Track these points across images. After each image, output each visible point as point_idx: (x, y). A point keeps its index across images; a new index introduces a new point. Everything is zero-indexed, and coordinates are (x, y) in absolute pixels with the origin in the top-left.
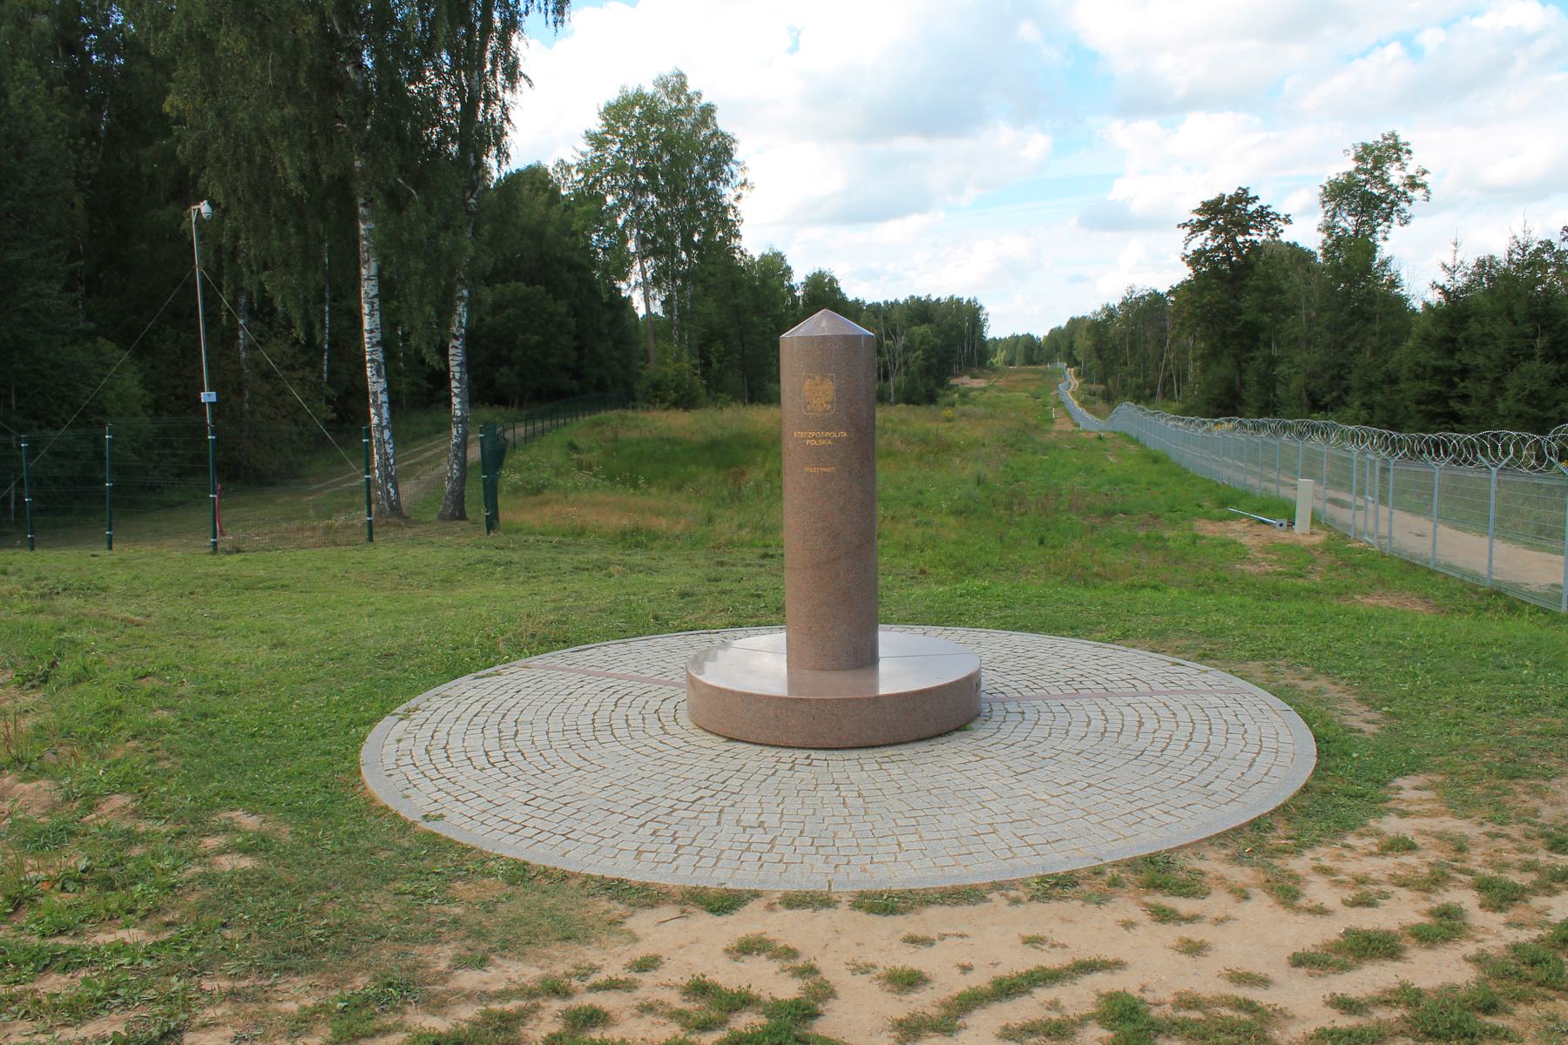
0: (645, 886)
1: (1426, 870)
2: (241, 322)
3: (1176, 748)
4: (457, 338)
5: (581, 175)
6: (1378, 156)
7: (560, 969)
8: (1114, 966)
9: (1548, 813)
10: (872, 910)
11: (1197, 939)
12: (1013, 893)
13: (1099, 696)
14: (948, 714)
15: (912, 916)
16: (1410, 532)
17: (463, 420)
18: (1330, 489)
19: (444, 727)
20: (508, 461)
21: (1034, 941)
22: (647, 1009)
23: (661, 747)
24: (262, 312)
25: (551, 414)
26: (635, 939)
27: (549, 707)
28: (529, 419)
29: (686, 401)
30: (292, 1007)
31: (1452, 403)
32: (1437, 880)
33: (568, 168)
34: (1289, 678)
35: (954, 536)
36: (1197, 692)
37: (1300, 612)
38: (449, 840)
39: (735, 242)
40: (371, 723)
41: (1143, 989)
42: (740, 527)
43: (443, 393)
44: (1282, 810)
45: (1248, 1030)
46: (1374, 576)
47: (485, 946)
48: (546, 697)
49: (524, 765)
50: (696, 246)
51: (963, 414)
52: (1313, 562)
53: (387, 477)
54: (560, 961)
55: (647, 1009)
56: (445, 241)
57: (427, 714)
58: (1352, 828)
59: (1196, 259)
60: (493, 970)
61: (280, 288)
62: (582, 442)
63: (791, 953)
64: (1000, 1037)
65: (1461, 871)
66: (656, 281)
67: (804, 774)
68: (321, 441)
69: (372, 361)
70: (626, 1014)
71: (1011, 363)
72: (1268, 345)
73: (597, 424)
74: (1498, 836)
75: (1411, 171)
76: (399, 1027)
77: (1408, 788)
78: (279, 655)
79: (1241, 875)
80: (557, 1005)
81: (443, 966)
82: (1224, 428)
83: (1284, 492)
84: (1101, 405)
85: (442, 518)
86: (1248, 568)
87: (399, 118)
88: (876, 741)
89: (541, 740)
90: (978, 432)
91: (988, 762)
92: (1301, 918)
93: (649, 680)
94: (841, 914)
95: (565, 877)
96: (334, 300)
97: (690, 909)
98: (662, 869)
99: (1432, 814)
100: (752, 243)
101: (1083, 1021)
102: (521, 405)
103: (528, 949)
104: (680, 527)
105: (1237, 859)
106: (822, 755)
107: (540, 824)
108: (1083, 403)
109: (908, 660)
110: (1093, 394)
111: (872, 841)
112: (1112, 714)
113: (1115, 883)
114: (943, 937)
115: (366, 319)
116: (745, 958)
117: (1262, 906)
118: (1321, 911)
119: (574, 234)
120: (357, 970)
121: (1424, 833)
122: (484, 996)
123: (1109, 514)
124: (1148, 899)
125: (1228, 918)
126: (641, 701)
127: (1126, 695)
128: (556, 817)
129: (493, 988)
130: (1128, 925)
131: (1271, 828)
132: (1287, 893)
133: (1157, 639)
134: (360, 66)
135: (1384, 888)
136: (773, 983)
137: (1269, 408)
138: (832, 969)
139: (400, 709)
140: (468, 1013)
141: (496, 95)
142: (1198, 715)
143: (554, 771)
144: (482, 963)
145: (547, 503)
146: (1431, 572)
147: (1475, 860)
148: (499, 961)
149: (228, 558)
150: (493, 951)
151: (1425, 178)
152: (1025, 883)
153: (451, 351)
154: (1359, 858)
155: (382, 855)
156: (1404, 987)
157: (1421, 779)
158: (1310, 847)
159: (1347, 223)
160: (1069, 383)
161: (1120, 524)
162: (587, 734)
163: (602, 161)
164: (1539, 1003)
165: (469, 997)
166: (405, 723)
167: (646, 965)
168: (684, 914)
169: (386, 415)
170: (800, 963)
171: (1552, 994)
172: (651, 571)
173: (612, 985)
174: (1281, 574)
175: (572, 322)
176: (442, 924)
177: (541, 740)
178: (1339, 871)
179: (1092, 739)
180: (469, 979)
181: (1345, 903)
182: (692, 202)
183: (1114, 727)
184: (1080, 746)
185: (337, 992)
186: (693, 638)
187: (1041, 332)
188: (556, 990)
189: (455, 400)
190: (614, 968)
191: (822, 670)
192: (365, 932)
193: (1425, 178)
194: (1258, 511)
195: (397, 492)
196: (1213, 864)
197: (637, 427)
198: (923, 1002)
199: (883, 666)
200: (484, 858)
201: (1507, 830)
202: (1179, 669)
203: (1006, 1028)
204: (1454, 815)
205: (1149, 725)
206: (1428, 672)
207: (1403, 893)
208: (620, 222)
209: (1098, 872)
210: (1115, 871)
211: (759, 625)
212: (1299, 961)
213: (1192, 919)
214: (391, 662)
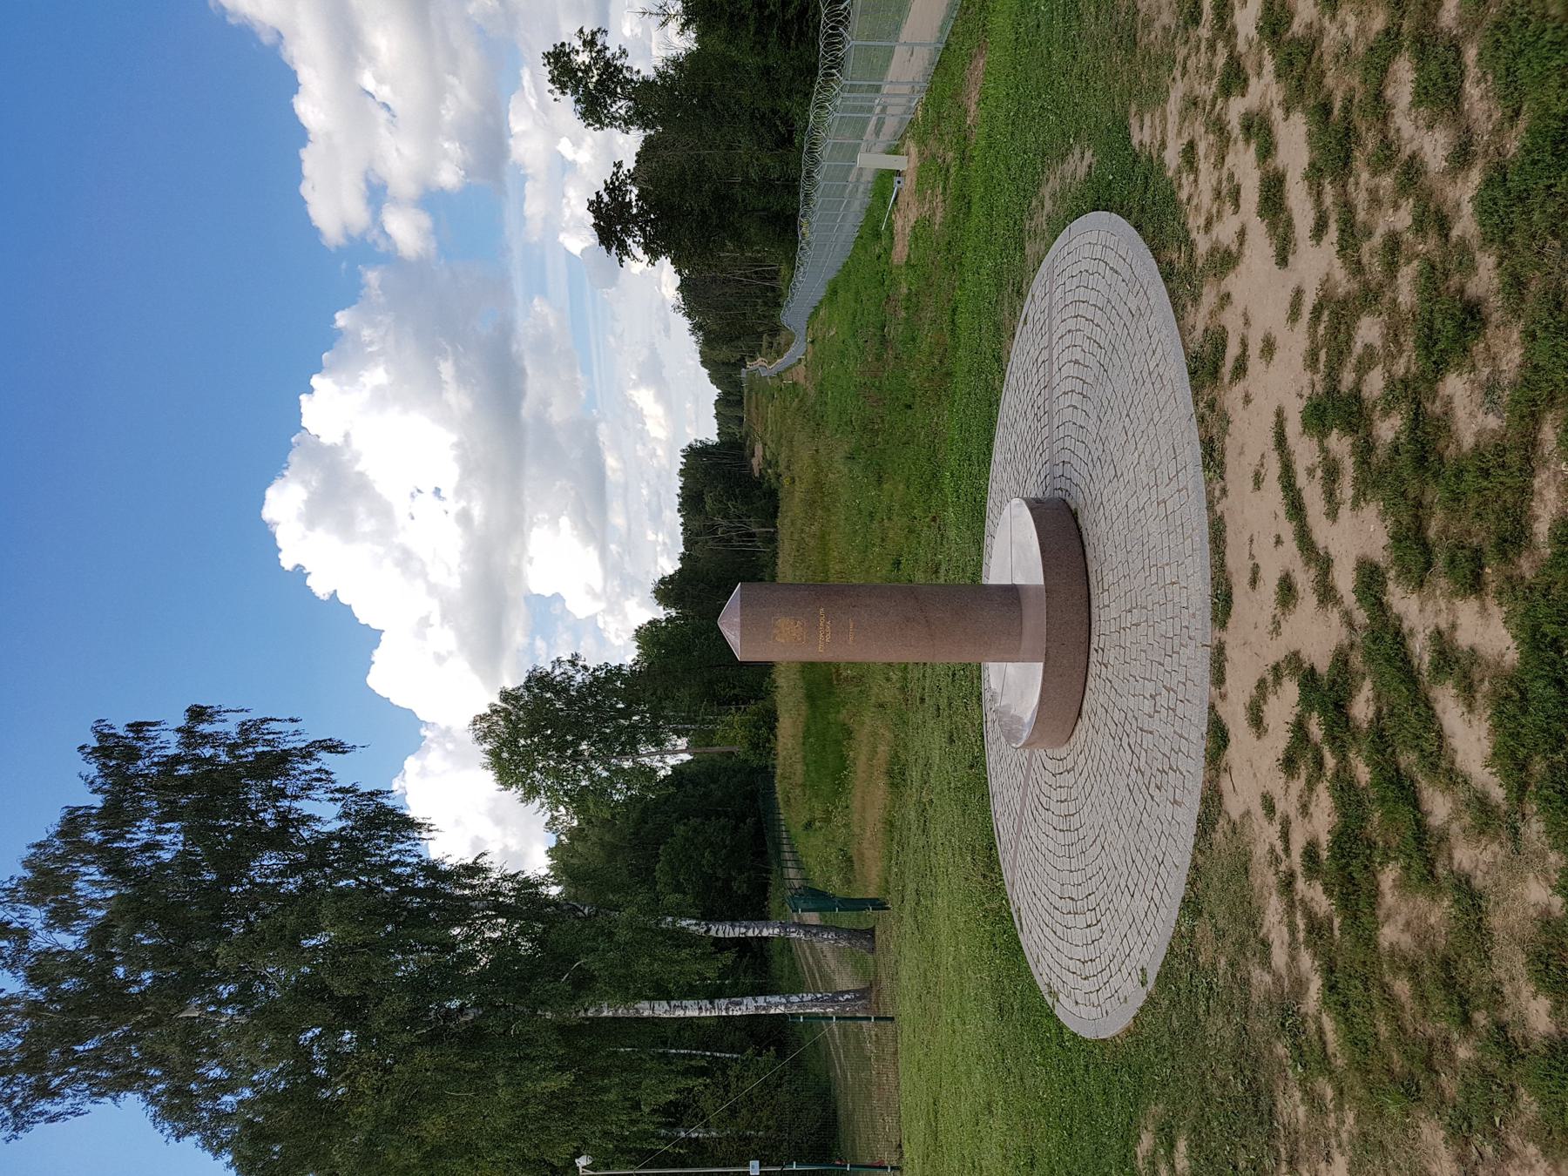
0: (1204, 800)
1: (1211, 137)
2: (683, 1134)
3: (1097, 334)
4: (709, 930)
5: (561, 808)
6: (561, 67)
7: (1272, 880)
8: (1279, 414)
9: (1166, 18)
10: (1227, 614)
11: (1261, 345)
12: (1217, 493)
13: (1051, 394)
14: (1061, 526)
15: (1234, 580)
16: (907, 67)
17: (783, 926)
18: (868, 139)
19: (1065, 962)
20: (821, 887)
21: (1258, 481)
22: (1304, 809)
23: (1085, 774)
24: (675, 1113)
25: (778, 846)
26: (1248, 813)
27: (1049, 868)
28: (781, 865)
29: (770, 719)
30: (1302, 1111)
31: (788, 17)
32: (1219, 126)
33: (554, 818)
34: (1041, 220)
35: (901, 487)
36: (1050, 307)
37: (982, 198)
38: (1163, 965)
39: (626, 670)
40: (1061, 1028)
41: (1301, 396)
42: (888, 680)
43: (754, 944)
44: (1156, 252)
45: (1335, 314)
46: (949, 102)
47: (1252, 941)
48: (1040, 869)
49: (1099, 894)
50: (628, 706)
51: (788, 468)
52: (934, 157)
53: (833, 1000)
54: (1265, 878)
55: (1304, 809)
56: (623, 935)
57: (1054, 977)
58: (1173, 193)
59: (653, 252)
60: (1272, 936)
61: (658, 1092)
62: (804, 817)
63: (1261, 684)
64: (1334, 521)
65: (1214, 106)
66: (659, 743)
67: (1111, 655)
68: (797, 1063)
69: (727, 1009)
70: (1309, 827)
71: (742, 419)
72: (730, 185)
73: (788, 801)
74: (1184, 68)
75: (577, 44)
76: (1318, 1020)
77: (1141, 135)
78: (999, 1110)
79: (1209, 297)
80: (1300, 884)
81: (1268, 978)
82: (810, 229)
83: (868, 177)
84: (782, 339)
85: (873, 950)
86: (938, 219)
87: (511, 976)
88: (1085, 592)
89: (1077, 877)
90: (805, 455)
91: (1105, 499)
92: (1247, 252)
93: (1026, 778)
94: (1231, 638)
95: (1195, 867)
96: (664, 1044)
97: (1223, 764)
98: (1188, 785)
99: (1164, 119)
100: (626, 654)
101: (1324, 450)
102: (768, 871)
103: (1254, 905)
104: (887, 733)
105: (1196, 299)
106: (1094, 639)
107: (1150, 886)
108: (779, 354)
109: (1013, 553)
110: (771, 345)
111: (1170, 605)
112: (1067, 385)
113: (1211, 406)
114: (1252, 556)
115: (689, 1013)
116: (1265, 722)
117: (1234, 283)
118: (1242, 234)
119: (613, 816)
120: (1271, 1052)
121: (1179, 133)
122: (1293, 945)
123: (884, 341)
124: (1226, 380)
125: (1245, 314)
126: (1045, 788)
127: (1051, 371)
128: (1144, 870)
129: (1286, 937)
130: (1247, 399)
131: (1171, 263)
132: (1226, 261)
133: (1002, 332)
134: (462, 1009)
135: (1225, 177)
136: (1285, 702)
137: (791, 186)
138: (1276, 652)
139: (1049, 1000)
140: (1306, 960)
141: (493, 885)
142: (1071, 311)
143: (1105, 868)
144: (1266, 944)
145: (862, 854)
146: (947, 48)
147: (1206, 91)
148: (1264, 930)
149: (907, 1156)
150: (1256, 934)
151: (587, 31)
152: (1209, 482)
153: (721, 935)
154: (1199, 191)
155: (1176, 1024)
156: (1306, 177)
157: (1134, 123)
158: (1188, 232)
159: (621, 107)
160: (760, 367)
161: (895, 331)
162: (1073, 837)
163: (549, 788)
164: (1324, 66)
165: (1293, 958)
166: (1061, 996)
167: (1269, 806)
168: (1228, 770)
169: (776, 999)
170: (1270, 678)
171: (1317, 53)
172: (928, 765)
173: (1285, 836)
174: (945, 188)
175: (693, 821)
176: (1233, 976)
177: (1077, 877)
178: (1209, 212)
179: (1088, 407)
180: (1279, 957)
181: (1235, 213)
182: (589, 709)
183: (1078, 386)
184: (1094, 418)
185: (1290, 1072)
186: (990, 737)
187: (714, 392)
188: (1288, 884)
189: (765, 933)
190: (1272, 832)
191: (1021, 634)
192: (1240, 1044)
193: (587, 31)
194: (885, 203)
195: (848, 992)
196: (1200, 318)
197: (791, 766)
198: (1304, 580)
199: (1019, 580)
200: (1178, 935)
201: (1180, 58)
202: (1030, 319)
203: (1327, 515)
204: (1166, 101)
205: (1079, 356)
206: (1039, 96)
207: (1229, 160)
208: (605, 774)
209: (1202, 419)
210: (1202, 405)
211: (979, 678)
212: (1282, 260)
213: (1244, 345)
214: (1007, 1006)
